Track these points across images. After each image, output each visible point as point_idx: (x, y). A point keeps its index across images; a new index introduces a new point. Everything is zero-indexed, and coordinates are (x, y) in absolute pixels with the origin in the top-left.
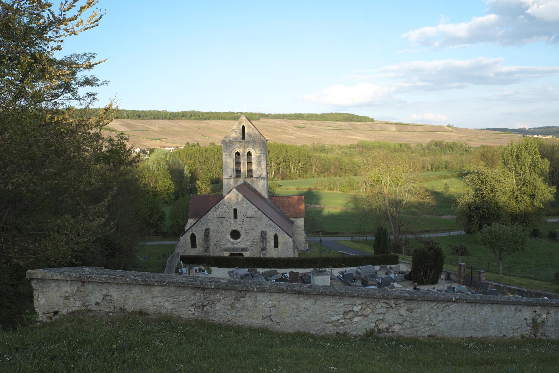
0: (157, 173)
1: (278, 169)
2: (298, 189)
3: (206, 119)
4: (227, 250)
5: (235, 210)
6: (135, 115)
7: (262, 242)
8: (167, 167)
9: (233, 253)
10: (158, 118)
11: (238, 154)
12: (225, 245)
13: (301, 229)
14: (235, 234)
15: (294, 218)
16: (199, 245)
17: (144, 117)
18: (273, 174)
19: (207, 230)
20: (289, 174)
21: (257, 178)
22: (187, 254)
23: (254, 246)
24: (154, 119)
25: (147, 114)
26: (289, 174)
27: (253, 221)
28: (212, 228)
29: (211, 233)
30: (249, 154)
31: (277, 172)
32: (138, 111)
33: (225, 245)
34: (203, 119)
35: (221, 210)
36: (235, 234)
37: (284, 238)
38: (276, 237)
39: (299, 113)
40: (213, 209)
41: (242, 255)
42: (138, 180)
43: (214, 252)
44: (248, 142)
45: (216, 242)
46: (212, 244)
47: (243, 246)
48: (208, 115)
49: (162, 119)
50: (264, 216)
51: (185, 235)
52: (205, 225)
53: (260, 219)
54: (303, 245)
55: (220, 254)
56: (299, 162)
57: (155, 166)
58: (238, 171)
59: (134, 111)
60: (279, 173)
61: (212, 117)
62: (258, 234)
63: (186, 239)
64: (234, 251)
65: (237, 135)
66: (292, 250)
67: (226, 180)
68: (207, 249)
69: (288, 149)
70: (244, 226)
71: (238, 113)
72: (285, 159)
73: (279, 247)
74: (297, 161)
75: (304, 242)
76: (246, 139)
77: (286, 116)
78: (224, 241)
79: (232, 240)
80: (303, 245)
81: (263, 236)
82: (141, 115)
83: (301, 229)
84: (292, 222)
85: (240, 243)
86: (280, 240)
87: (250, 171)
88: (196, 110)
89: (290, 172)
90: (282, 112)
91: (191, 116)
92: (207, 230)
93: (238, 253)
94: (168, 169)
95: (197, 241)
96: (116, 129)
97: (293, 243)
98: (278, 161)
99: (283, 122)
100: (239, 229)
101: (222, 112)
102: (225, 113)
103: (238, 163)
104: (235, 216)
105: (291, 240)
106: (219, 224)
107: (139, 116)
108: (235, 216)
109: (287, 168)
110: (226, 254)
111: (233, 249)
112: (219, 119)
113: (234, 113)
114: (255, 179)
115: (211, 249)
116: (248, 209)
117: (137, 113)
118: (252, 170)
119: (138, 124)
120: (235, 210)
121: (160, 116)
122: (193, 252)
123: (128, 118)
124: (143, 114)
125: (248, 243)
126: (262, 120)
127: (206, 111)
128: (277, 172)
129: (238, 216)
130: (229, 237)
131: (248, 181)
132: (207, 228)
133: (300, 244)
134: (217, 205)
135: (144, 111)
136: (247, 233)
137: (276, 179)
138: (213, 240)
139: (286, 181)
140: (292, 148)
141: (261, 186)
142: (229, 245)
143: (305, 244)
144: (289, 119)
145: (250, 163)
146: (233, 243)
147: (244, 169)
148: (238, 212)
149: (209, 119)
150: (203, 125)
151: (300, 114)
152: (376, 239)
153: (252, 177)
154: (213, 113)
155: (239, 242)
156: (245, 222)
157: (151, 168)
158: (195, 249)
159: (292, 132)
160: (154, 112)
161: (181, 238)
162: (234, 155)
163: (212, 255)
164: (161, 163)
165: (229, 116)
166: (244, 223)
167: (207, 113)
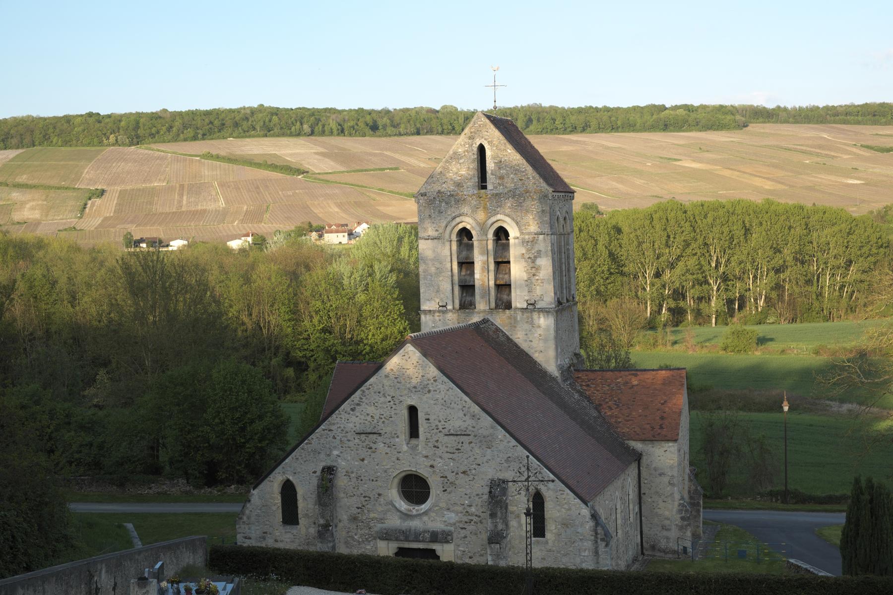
0: (361, 297)
1: (778, 287)
2: (817, 353)
3: (574, 130)
4: (387, 535)
5: (413, 411)
6: (361, 124)
7: (493, 515)
8: (392, 279)
9: (407, 545)
10: (430, 132)
11: (465, 233)
12: (381, 520)
13: (666, 479)
14: (415, 488)
15: (643, 440)
16: (306, 516)
17: (390, 130)
18: (761, 303)
19: (329, 471)
20: (816, 304)
21: (523, 310)
22: (270, 543)
23: (471, 527)
24: (418, 133)
25: (397, 119)
26: (816, 304)
27: (466, 446)
28: (342, 464)
29: (341, 481)
30: (501, 234)
31: (774, 295)
32: (370, 112)
33: (381, 520)
34: (565, 131)
35: (371, 410)
36: (415, 488)
37: (561, 504)
38: (538, 500)
39: (848, 103)
40: (346, 406)
41: (432, 553)
42: (220, 314)
43: (349, 543)
44: (497, 195)
45: (354, 511)
46: (343, 516)
47: (436, 524)
48: (582, 118)
49: (442, 133)
50: (501, 433)
51: (265, 485)
52: (322, 456)
53: (488, 442)
54: (674, 533)
55: (367, 549)
56: (849, 263)
57: (357, 275)
58: (467, 288)
59: (360, 111)
60: (780, 297)
61: (594, 123)
62: (481, 487)
63: (269, 492)
64: (407, 540)
65: (465, 169)
66: (589, 544)
67: (429, 317)
68: (325, 530)
69: (813, 220)
70: (439, 463)
71: (676, 108)
72: (800, 252)
73: (548, 535)
74: (842, 261)
75: (679, 522)
76: (490, 187)
77: (836, 114)
78: (380, 509)
79: (403, 505)
80: (674, 533)
81: (497, 494)
82: (380, 123)
83: (666, 479)
84: (638, 457)
85: (431, 516)
86: (551, 511)
87: (503, 287)
88: (546, 104)
89: (820, 295)
90: (793, 100)
91: (530, 121)
92: (329, 471)
93: (421, 546)
94: (399, 284)
95: (301, 504)
96: (307, 166)
97: (591, 524)
98: (778, 261)
99: (824, 134)
100: (423, 471)
101: (625, 105)
102: (635, 109)
103: (466, 264)
104: (414, 432)
105: (585, 512)
106: (363, 453)
107: (374, 128)
108: (414, 432)
109: (809, 282)
110: (386, 549)
111: (406, 535)
112: (614, 128)
113: (663, 108)
114: (519, 316)
115: (340, 533)
116: (449, 407)
117: (368, 118)
118: (473, 287)
119: (369, 150)
120: (413, 411)
121: (434, 123)
122: (287, 539)
123: (342, 132)
124: (386, 120)
125: (452, 517)
126: (754, 127)
127: (575, 105)
128: (774, 295)
129: (421, 430)
130: (394, 494)
131: (500, 320)
132: (329, 463)
133: (664, 528)
134: (358, 393)
135: (387, 112)
136: (448, 486)
137: (771, 319)
138: (346, 503)
139: (806, 325)
140: (828, 218)
141: (539, 339)
142: (394, 522)
143: (681, 528)
144: (845, 122)
145: (502, 264)
146: (406, 516)
147: (483, 275)
148: (421, 416)
149: (584, 130)
150: (565, 148)
151: (883, 105)
152: (849, 519)
153: (508, 306)
154: (597, 110)
155: (426, 513)
156: (443, 449)
157: (346, 282)
158: (294, 530)
159: (855, 164)
160: (418, 111)
161: (255, 492)
162: (454, 237)
163: (342, 550)
164: (376, 267)
165: (647, 117)
166: (438, 452)
167: (580, 111)
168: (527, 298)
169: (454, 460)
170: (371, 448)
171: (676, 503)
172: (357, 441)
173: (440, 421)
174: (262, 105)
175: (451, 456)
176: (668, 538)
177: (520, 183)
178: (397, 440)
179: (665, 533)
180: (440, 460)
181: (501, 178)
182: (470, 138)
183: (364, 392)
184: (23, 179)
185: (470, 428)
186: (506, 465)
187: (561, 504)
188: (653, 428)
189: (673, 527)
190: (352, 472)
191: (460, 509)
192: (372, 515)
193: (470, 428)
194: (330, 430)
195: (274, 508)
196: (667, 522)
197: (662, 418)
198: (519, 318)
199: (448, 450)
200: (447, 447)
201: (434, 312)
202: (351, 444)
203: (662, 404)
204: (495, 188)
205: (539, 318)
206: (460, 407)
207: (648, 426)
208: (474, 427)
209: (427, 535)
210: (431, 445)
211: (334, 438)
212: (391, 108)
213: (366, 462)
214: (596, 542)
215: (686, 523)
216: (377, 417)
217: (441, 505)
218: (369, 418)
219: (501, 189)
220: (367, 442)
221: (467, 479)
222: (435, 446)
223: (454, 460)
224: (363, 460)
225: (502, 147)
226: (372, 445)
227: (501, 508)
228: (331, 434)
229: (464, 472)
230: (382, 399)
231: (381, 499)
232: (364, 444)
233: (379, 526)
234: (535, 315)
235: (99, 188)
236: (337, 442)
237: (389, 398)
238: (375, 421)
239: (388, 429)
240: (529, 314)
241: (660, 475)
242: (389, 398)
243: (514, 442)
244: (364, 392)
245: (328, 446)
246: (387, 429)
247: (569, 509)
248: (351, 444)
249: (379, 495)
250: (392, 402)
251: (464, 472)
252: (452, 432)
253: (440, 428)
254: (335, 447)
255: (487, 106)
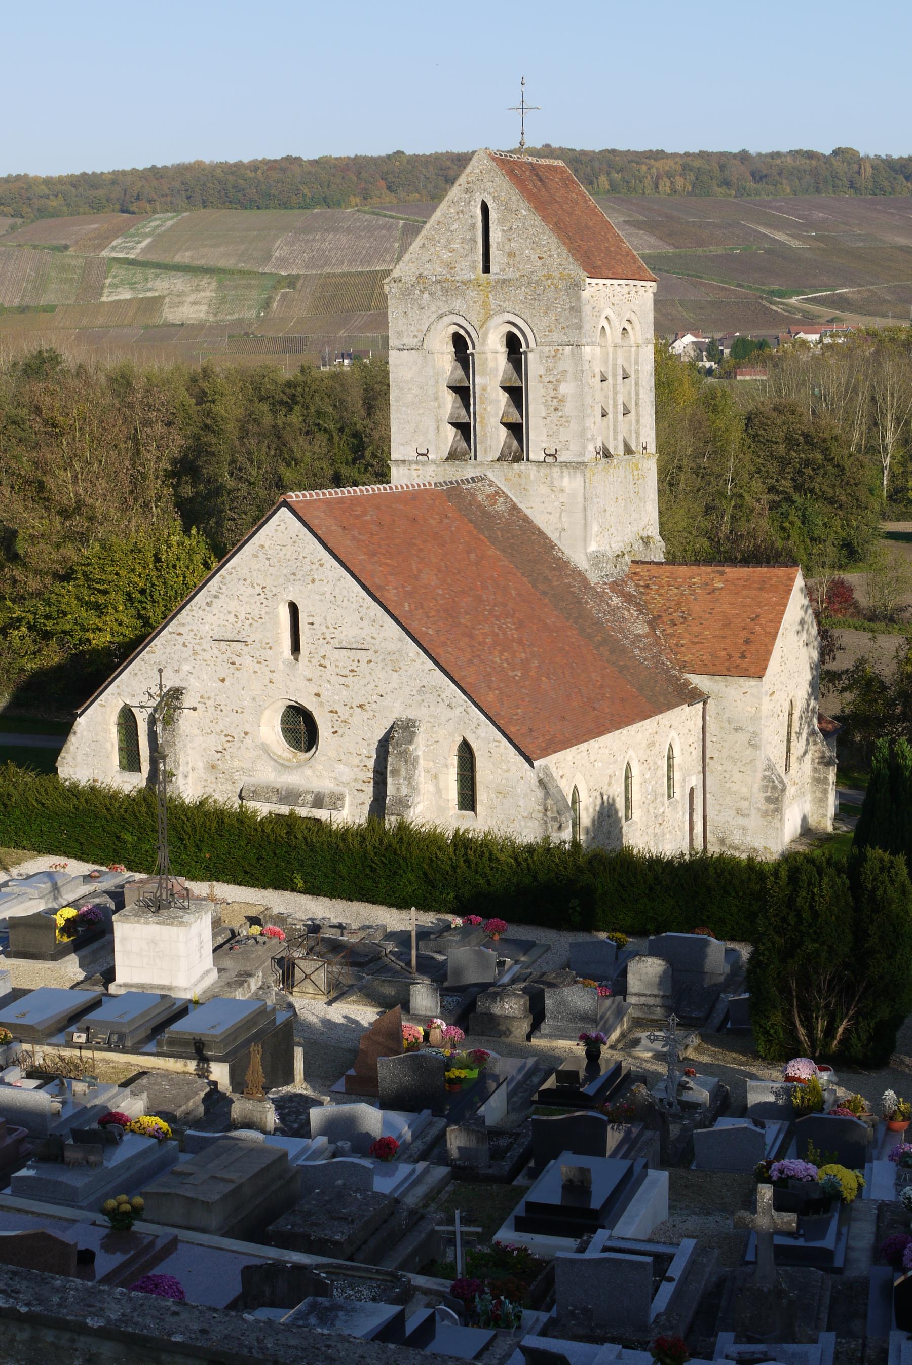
27: (363, 664)
47: (325, 784)
73: (479, 808)
106: (224, 670)
131: (501, 478)
135: (744, 156)
168: (544, 445)
169: (347, 686)
170: (233, 663)
171: (759, 775)
172: (215, 651)
173: (328, 627)
174: (890, 156)
175: (342, 680)
176: (744, 829)
177: (540, 263)
178: (269, 652)
179: (741, 821)
180: (327, 685)
181: (511, 254)
182: (467, 191)
183: (224, 578)
184: (184, 257)
185: (368, 639)
186: (419, 698)
187: (497, 760)
188: (730, 656)
189: (753, 812)
190: (209, 698)
191: (356, 761)
192: (236, 763)
193: (368, 639)
194: (181, 634)
195: (108, 745)
196: (744, 805)
197: (747, 642)
198: (532, 477)
199: (338, 671)
200: (337, 666)
201: (410, 463)
202: (207, 656)
203: (753, 620)
204: (503, 270)
205: (562, 477)
206: (354, 606)
207: (723, 653)
208: (373, 638)
209: (310, 798)
210: (315, 662)
211: (184, 645)
212: (753, 150)
213: (226, 682)
214: (546, 822)
215: (772, 806)
216: (242, 617)
217: (330, 754)
218: (232, 619)
219: (510, 274)
220: (229, 654)
221: (366, 715)
222: (321, 665)
223: (347, 686)
224: (223, 680)
225: (514, 207)
226: (235, 659)
227: (406, 762)
228: (181, 640)
229: (361, 706)
230: (250, 590)
231: (248, 740)
232: (225, 657)
233: (245, 778)
234: (556, 471)
235: (294, 273)
236: (188, 652)
237: (258, 590)
238: (240, 624)
239: (257, 636)
240: (548, 470)
241: (736, 730)
242: (258, 590)
243: (430, 664)
244: (224, 578)
245: (176, 658)
246: (254, 636)
247: (508, 771)
248: (207, 656)
249: (246, 734)
250: (263, 595)
251: (361, 706)
252: (344, 644)
253: (328, 637)
254: (186, 660)
255: (507, 142)
